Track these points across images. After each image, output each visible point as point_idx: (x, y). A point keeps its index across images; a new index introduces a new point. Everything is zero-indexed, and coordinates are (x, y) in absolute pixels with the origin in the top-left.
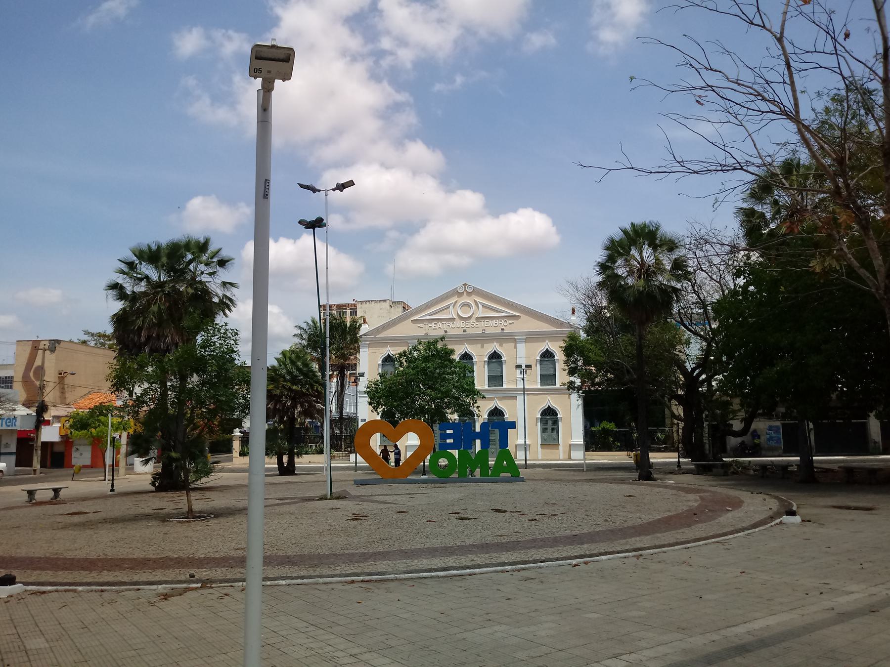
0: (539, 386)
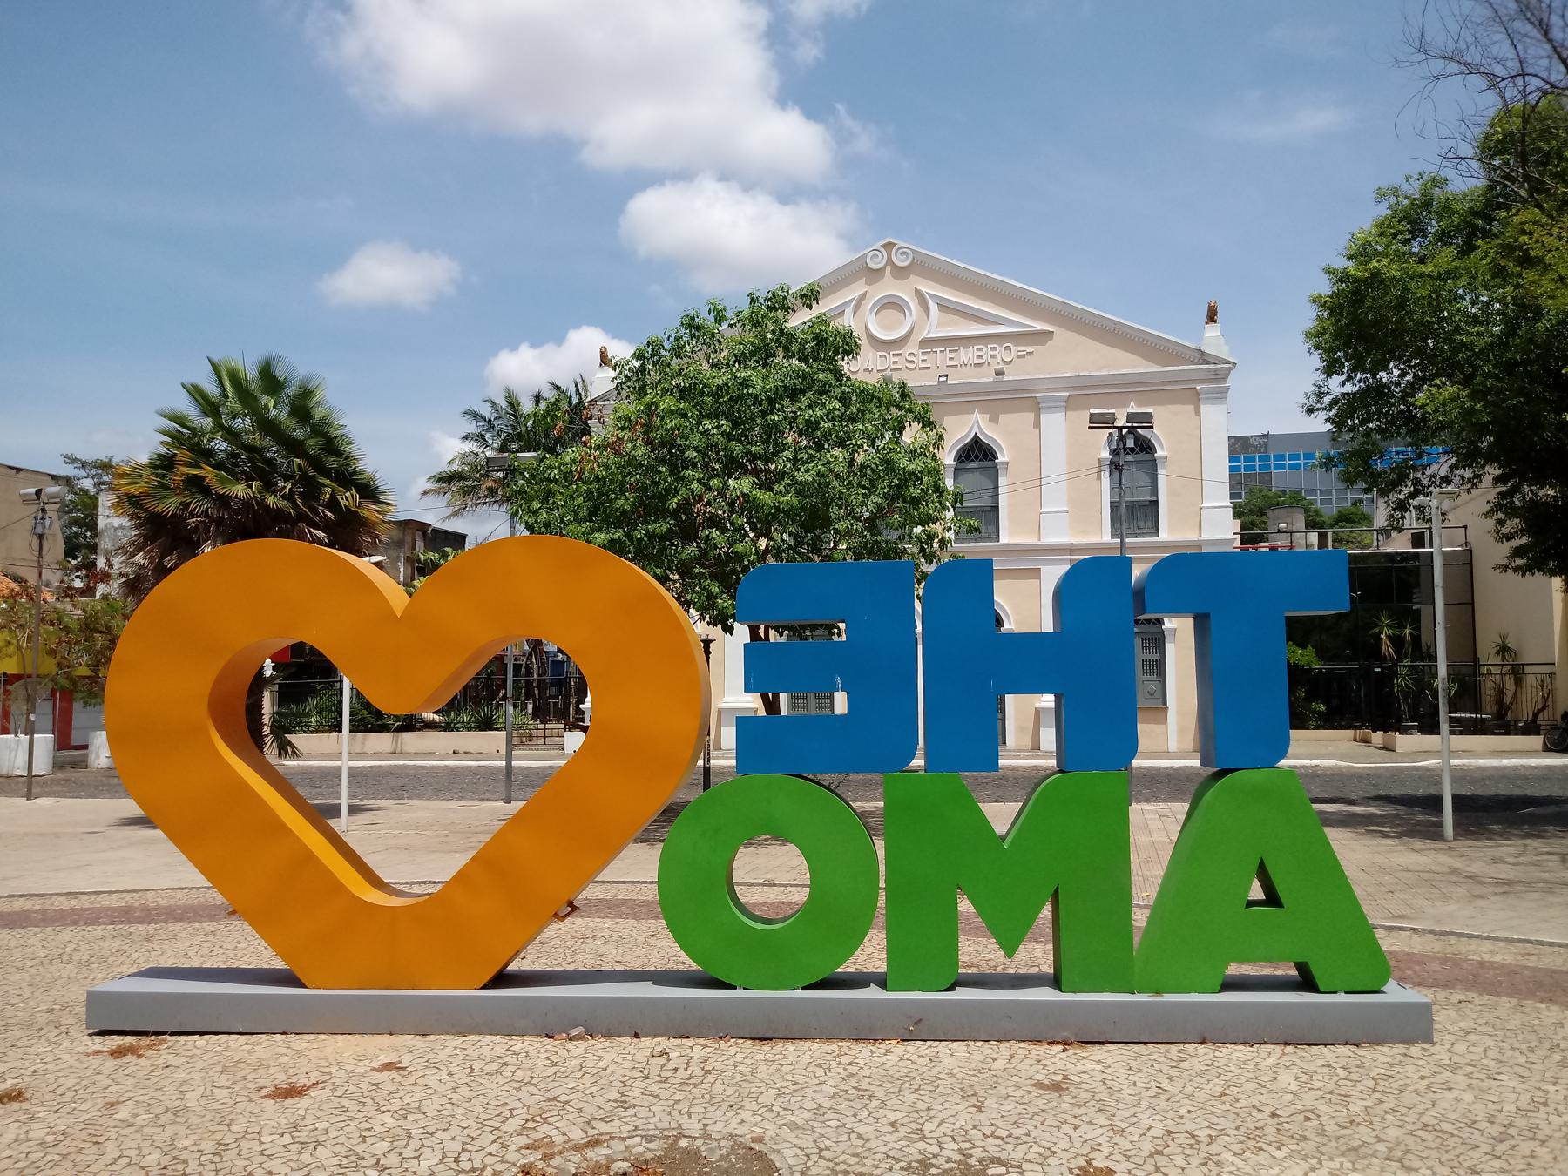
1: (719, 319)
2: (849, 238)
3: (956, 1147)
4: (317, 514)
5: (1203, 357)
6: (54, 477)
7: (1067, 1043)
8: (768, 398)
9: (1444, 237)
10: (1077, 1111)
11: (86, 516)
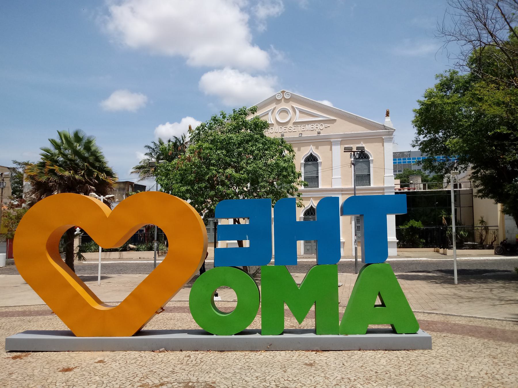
1: (224, 117)
2: (275, 88)
3: (275, 384)
4: (92, 181)
5: (385, 127)
6: (9, 168)
7: (317, 351)
8: (238, 143)
9: (457, 91)
10: (316, 372)
11: (20, 181)
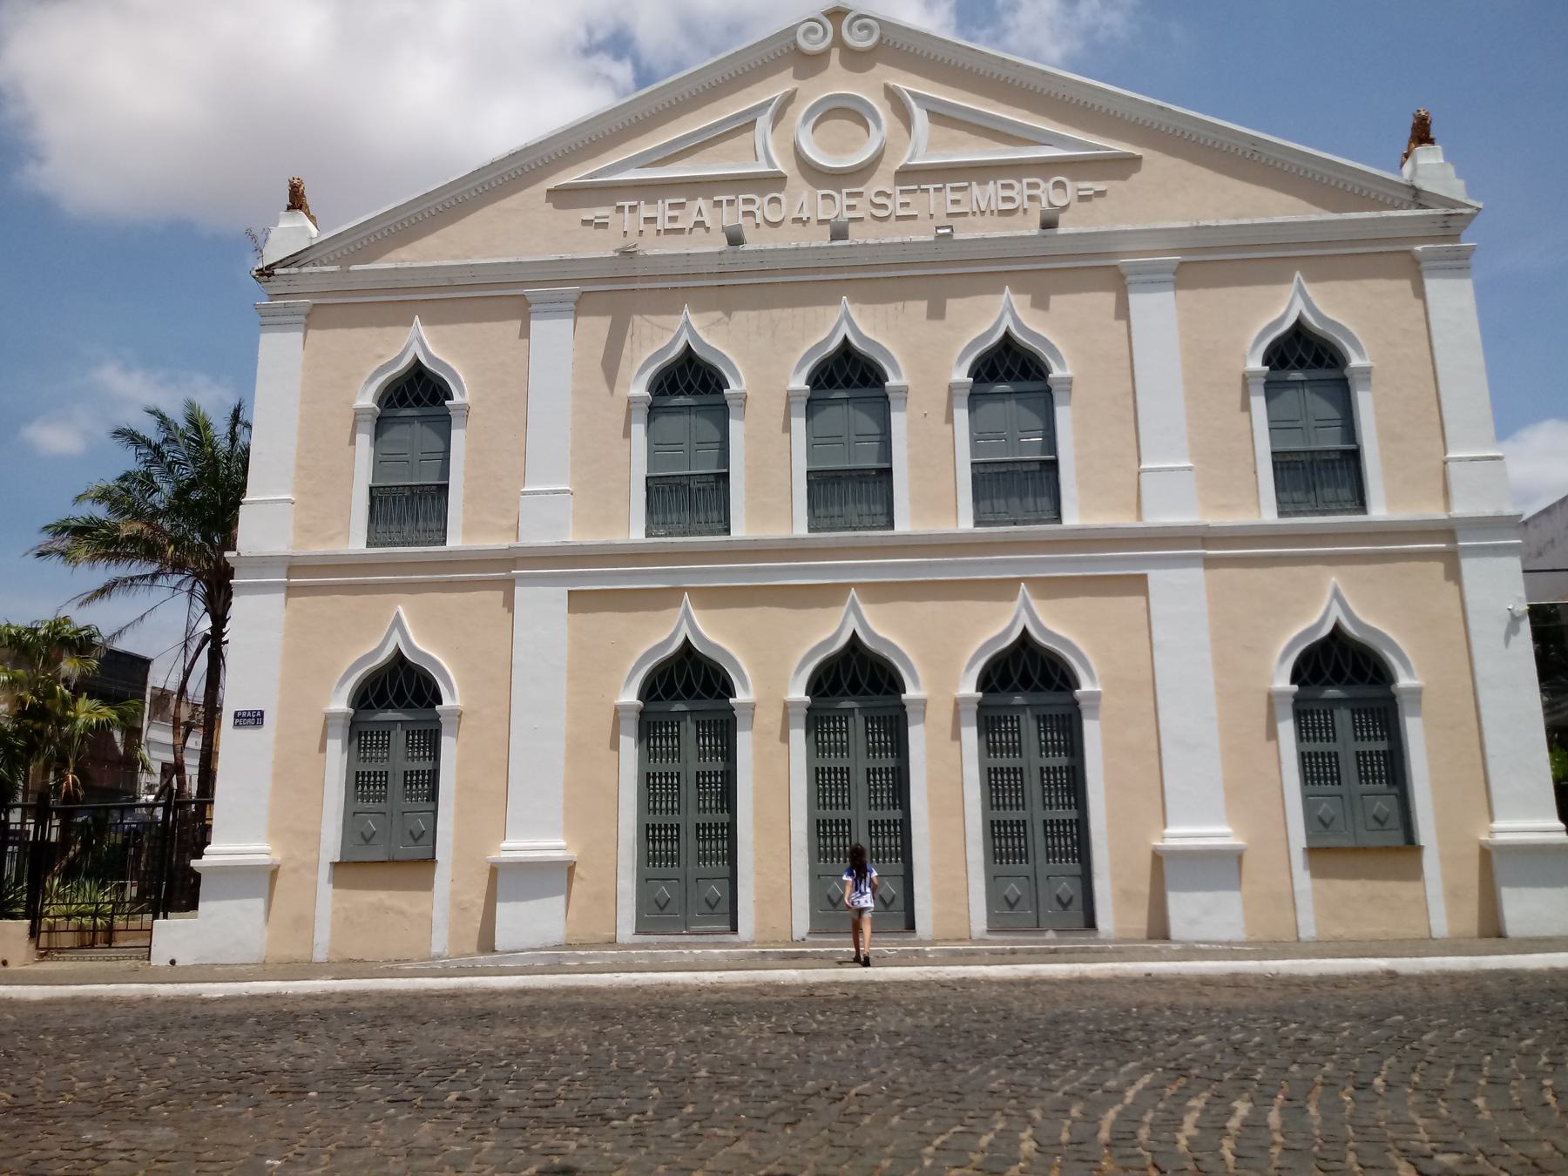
0: (1268, 515)
5: (1416, 196)
